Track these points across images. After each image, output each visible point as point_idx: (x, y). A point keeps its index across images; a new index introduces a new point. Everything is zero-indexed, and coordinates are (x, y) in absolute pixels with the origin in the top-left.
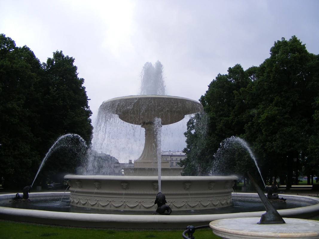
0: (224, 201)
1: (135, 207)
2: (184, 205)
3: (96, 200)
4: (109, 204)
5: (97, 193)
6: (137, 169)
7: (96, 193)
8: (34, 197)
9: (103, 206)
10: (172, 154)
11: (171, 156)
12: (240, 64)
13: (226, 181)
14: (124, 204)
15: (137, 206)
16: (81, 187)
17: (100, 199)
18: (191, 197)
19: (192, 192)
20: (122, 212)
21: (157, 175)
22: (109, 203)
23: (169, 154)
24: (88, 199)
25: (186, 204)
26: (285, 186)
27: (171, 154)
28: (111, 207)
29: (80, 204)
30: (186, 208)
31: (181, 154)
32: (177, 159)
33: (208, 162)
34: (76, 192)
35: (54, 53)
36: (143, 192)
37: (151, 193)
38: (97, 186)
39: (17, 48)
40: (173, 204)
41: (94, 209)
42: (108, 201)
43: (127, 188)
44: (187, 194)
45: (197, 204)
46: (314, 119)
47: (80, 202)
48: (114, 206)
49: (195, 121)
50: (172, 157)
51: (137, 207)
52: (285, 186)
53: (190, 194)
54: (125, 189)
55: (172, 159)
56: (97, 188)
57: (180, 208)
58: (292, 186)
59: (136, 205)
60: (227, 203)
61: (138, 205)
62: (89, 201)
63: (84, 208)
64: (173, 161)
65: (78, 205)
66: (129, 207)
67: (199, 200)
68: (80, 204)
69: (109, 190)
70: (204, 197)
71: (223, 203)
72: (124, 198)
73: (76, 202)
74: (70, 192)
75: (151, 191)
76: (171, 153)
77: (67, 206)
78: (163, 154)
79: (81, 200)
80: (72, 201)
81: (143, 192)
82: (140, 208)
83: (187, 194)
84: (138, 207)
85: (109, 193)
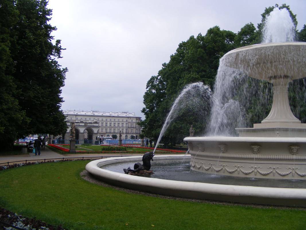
1: (268, 174)
3: (201, 163)
4: (236, 170)
5: (257, 159)
6: (290, 130)
7: (222, 157)
8: (166, 159)
9: (230, 173)
10: (77, 113)
11: (76, 115)
12: (218, 26)
14: (224, 169)
16: (291, 152)
18: (220, 161)
19: (299, 157)
20: (254, 181)
22: (238, 169)
23: (74, 114)
24: (202, 163)
25: (294, 172)
27: (76, 114)
28: (239, 173)
29: (202, 169)
31: (86, 114)
32: (106, 119)
34: (198, 156)
36: (286, 156)
37: (279, 157)
38: (222, 149)
40: (258, 170)
41: (268, 180)
42: (236, 167)
43: (258, 152)
46: (187, 87)
48: (243, 173)
49: (158, 82)
50: (77, 117)
51: (252, 173)
54: (223, 153)
55: (77, 118)
56: (222, 151)
57: (246, 174)
58: (176, 145)
63: (247, 178)
64: (115, 122)
65: (200, 171)
68: (202, 169)
69: (247, 154)
70: (188, 160)
72: (219, 161)
74: (190, 155)
75: (282, 156)
76: (76, 112)
77: (186, 171)
78: (68, 114)
79: (203, 165)
82: (256, 175)
83: (252, 158)
84: (271, 174)
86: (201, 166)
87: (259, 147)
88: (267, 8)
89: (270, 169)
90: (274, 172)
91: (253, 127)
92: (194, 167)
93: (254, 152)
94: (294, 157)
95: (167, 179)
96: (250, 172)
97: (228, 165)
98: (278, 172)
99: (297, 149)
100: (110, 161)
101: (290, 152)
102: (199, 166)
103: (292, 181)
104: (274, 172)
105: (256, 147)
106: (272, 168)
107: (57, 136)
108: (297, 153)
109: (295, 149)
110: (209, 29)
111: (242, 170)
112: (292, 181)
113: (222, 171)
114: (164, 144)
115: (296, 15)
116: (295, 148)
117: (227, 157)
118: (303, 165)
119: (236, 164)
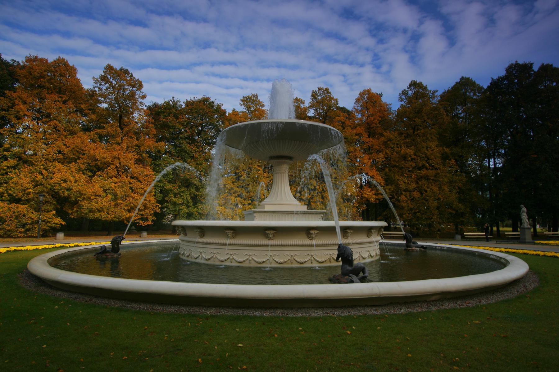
0: (21, 245)
1: (244, 261)
2: (289, 260)
9: (207, 260)
13: (369, 231)
14: (231, 258)
15: (227, 259)
16: (267, 237)
17: (218, 251)
21: (332, 219)
26: (484, 234)
28: (214, 261)
30: (292, 263)
33: (359, 203)
35: (257, 96)
39: (488, 87)
41: (242, 267)
42: (228, 255)
44: (267, 246)
45: (246, 259)
47: (202, 256)
52: (484, 234)
53: (271, 245)
57: (260, 263)
59: (227, 258)
60: (372, 257)
61: (247, 259)
62: (203, 254)
66: (237, 261)
67: (231, 253)
71: (364, 256)
73: (187, 254)
79: (192, 253)
80: (182, 253)
81: (292, 242)
85: (215, 244)
86: (190, 254)
87: (274, 232)
88: (495, 79)
89: (288, 256)
90: (250, 258)
91: (264, 209)
92: (183, 254)
93: (228, 237)
94: (314, 242)
95: (245, 284)
96: (244, 259)
97: (277, 255)
98: (296, 259)
99: (316, 234)
100: (137, 249)
101: (344, 236)
102: (188, 254)
103: (221, 266)
104: (250, 258)
105: (272, 232)
106: (248, 255)
107: (422, 171)
108: (274, 237)
109: (314, 234)
110: (507, 66)
111: (275, 259)
112: (221, 266)
113: (229, 260)
114: (64, 223)
115: (234, 109)
116: (270, 233)
117: (332, 245)
118: (263, 251)
119: (212, 250)
